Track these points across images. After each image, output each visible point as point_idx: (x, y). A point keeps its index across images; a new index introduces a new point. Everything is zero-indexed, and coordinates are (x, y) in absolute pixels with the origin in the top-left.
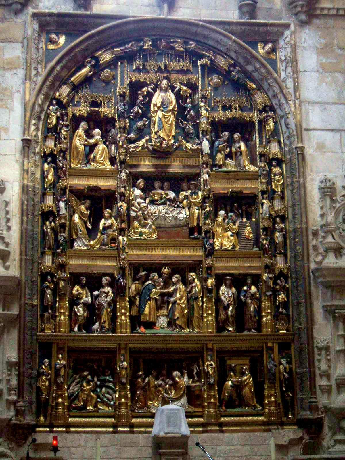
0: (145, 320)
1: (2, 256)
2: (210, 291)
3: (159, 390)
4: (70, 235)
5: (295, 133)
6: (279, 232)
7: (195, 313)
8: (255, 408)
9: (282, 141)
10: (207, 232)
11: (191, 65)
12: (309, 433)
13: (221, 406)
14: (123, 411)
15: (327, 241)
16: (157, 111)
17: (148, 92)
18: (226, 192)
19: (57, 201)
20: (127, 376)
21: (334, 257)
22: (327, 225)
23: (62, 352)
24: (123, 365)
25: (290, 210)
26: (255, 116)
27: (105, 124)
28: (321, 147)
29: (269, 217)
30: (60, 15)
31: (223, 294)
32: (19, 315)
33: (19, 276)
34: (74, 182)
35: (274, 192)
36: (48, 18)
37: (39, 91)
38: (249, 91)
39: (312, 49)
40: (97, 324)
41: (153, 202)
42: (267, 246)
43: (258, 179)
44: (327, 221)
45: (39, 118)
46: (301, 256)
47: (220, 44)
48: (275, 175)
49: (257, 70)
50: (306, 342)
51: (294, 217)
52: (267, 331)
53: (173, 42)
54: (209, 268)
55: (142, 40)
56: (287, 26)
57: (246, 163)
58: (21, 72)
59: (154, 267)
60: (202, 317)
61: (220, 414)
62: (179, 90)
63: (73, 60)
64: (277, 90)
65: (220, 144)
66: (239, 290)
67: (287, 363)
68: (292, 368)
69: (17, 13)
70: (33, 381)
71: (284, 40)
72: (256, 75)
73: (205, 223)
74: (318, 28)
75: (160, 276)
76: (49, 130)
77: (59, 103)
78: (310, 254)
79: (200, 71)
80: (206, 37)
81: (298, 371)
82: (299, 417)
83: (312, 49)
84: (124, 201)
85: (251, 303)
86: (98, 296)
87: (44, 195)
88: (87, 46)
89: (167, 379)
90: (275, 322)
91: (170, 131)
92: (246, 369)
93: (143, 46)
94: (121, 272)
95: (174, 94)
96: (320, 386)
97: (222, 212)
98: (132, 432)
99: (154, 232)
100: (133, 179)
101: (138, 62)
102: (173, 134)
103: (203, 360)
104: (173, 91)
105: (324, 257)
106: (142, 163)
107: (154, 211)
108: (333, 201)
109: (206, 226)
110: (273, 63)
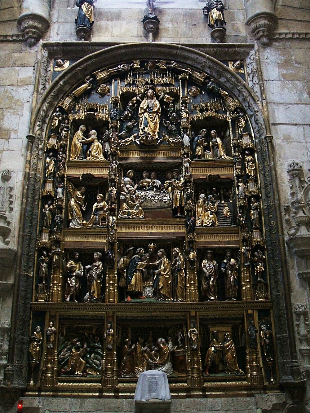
0: (131, 290)
1: (4, 233)
2: (192, 263)
3: (145, 356)
4: (67, 216)
5: (263, 127)
6: (254, 210)
7: (178, 283)
8: (238, 373)
9: (253, 135)
10: (188, 211)
11: (173, 80)
12: (292, 398)
13: (204, 371)
14: (109, 376)
15: (298, 216)
16: (143, 113)
17: (137, 100)
18: (205, 177)
19: (55, 187)
20: (113, 342)
21: (306, 230)
22: (298, 201)
23: (54, 319)
24: (109, 331)
25: (263, 191)
26: (229, 117)
27: (101, 127)
28: (287, 138)
29: (245, 197)
30: (64, 44)
31: (205, 266)
32: (13, 285)
33: (17, 250)
34: (73, 172)
35: (248, 176)
36: (55, 48)
37: (44, 100)
38: (223, 98)
39: (274, 64)
40: (88, 294)
41: (140, 188)
42: (243, 222)
43: (233, 167)
44: (297, 199)
45: (44, 122)
46: (276, 230)
47: (197, 62)
48: (248, 162)
49: (228, 80)
50: (284, 308)
51: (267, 196)
52: (246, 299)
53: (157, 62)
54: (191, 242)
55: (133, 62)
56: (252, 47)
57: (223, 153)
58: (31, 88)
59: (143, 243)
60: (185, 287)
61: (203, 378)
62: (163, 98)
63: (74, 78)
64: (245, 93)
65: (199, 139)
66: (220, 263)
67: (267, 329)
68: (272, 332)
69: (31, 45)
70: (25, 346)
71: (250, 58)
72: (228, 85)
73: (187, 204)
74: (278, 49)
75: (147, 251)
76: (52, 131)
77: (62, 110)
78: (284, 228)
79: (180, 84)
80: (185, 58)
81: (278, 336)
82: (281, 381)
83: (274, 64)
84: (115, 186)
85: (231, 274)
86: (90, 269)
87: (45, 182)
88: (86, 66)
89: (154, 345)
90: (254, 291)
91: (155, 128)
92: (228, 335)
93: (133, 66)
94: (110, 248)
95: (159, 101)
96: (300, 350)
97: (202, 195)
98: (117, 397)
99: (141, 213)
100: (123, 169)
101: (130, 79)
102: (158, 131)
103: (186, 328)
104: (157, 99)
105: (297, 230)
106: (131, 156)
107: (142, 195)
108: (301, 182)
109: (187, 205)
110: (243, 75)
